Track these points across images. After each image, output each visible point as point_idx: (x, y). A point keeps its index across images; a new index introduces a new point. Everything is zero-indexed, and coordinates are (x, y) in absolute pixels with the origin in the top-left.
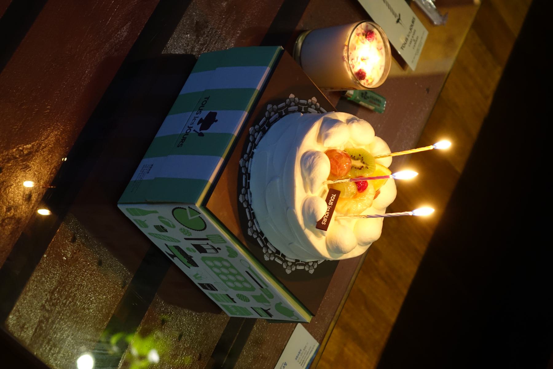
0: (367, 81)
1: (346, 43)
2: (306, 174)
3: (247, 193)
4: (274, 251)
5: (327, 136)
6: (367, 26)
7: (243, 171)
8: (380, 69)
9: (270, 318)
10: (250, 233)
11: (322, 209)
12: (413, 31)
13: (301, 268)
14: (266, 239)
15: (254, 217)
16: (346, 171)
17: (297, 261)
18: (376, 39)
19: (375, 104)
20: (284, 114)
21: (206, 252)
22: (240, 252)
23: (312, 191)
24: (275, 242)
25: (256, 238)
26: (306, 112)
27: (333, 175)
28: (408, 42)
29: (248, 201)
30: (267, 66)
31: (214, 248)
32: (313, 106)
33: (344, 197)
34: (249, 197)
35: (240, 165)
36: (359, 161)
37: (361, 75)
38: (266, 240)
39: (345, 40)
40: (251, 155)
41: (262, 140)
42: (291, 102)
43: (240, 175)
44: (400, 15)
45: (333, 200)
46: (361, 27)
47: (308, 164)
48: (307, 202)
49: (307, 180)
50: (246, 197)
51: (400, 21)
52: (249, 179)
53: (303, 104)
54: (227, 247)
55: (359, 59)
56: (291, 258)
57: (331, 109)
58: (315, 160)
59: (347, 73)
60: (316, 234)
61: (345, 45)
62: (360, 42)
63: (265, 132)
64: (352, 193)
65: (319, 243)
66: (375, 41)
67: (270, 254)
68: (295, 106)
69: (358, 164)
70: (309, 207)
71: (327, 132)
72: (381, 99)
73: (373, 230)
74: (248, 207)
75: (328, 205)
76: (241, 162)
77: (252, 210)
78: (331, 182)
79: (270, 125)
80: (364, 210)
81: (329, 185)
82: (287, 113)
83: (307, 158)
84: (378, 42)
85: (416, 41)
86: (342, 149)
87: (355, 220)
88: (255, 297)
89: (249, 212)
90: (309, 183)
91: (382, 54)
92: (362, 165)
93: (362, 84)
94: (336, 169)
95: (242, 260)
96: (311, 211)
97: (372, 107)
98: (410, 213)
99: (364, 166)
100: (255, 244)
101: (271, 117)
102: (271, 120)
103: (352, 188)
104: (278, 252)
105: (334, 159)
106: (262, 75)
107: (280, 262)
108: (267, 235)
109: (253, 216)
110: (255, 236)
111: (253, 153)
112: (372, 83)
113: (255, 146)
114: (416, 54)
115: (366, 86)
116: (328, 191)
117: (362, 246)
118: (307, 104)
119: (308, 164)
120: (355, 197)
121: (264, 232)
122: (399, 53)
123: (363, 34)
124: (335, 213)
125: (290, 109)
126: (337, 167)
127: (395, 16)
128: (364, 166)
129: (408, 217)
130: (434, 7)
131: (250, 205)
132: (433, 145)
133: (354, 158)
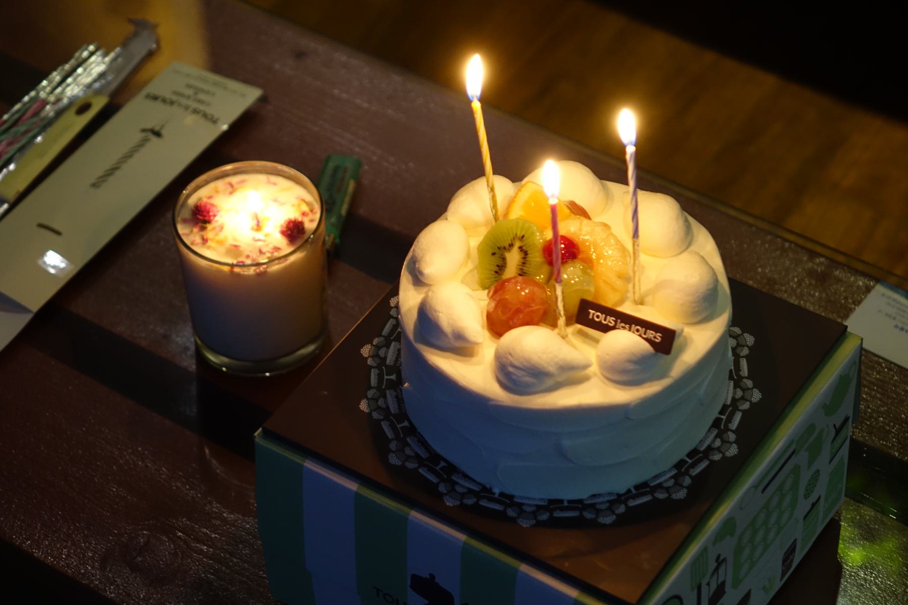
0: (304, 214)
1: (226, 269)
2: (550, 382)
3: (592, 506)
4: (715, 432)
5: (459, 336)
6: (185, 221)
7: (545, 517)
8: (275, 184)
9: (851, 419)
10: (681, 494)
11: (624, 341)
12: (174, 98)
13: (744, 364)
14: (690, 455)
15: (645, 484)
16: (536, 289)
17: (731, 377)
18: (210, 197)
19: (343, 179)
20: (406, 424)
21: (723, 583)
22: (726, 512)
23: (586, 366)
24: (699, 434)
25: (691, 477)
26: (396, 369)
27: (544, 316)
28: (201, 107)
29: (611, 502)
30: (302, 466)
31: (717, 569)
32: (382, 353)
33: (592, 289)
34: (601, 500)
35: (532, 526)
36: (508, 255)
37: (294, 231)
38: (693, 453)
39: (221, 271)
40: (507, 499)
41: (471, 475)
42: (379, 408)
43: (554, 523)
44: (144, 131)
45: (602, 317)
46: (187, 235)
47: (528, 379)
48: (610, 376)
49: (560, 379)
50: (604, 507)
51: (157, 129)
52: (561, 501)
53: (380, 377)
54: (714, 544)
55: (259, 235)
56: (728, 393)
57: (397, 332)
58: (516, 363)
59: (293, 264)
60: (682, 349)
61: (232, 272)
62: (221, 236)
63: (452, 469)
64: (584, 271)
65: (700, 340)
66: (214, 201)
67: (723, 441)
68: (385, 397)
69: (513, 258)
70: (624, 372)
71: (450, 336)
72: (331, 165)
73: (660, 213)
74: (625, 502)
75: (614, 328)
76: (525, 524)
77: (629, 491)
78: (562, 321)
79: (435, 458)
80: (618, 241)
81: (568, 323)
82: (403, 415)
83: (514, 382)
84: (217, 192)
85: (197, 91)
86: (484, 295)
87: (643, 258)
88: (810, 463)
89: (634, 497)
90: (571, 374)
91: (243, 182)
92: (515, 249)
93: (314, 225)
94: (532, 311)
95: (740, 506)
96: (631, 367)
97: (351, 186)
98: (630, 150)
99: (517, 244)
100: (704, 480)
101: (388, 407)
102: (423, 454)
103: (571, 273)
104: (716, 423)
105: (511, 318)
106: (324, 477)
107: (738, 417)
108: (682, 454)
109: (642, 488)
110: (687, 481)
111: (502, 494)
112: (307, 204)
113: (486, 491)
114: (225, 88)
115: (318, 216)
116: (579, 326)
117: (693, 236)
118: (378, 367)
119: (528, 379)
120: (589, 263)
121: (675, 460)
122: (225, 127)
123: (203, 229)
124: (627, 309)
125: (393, 408)
126: (527, 310)
127: (145, 140)
128: (517, 244)
129: (638, 155)
130: (118, 50)
131: (619, 496)
132: (470, 102)
133: (501, 267)
